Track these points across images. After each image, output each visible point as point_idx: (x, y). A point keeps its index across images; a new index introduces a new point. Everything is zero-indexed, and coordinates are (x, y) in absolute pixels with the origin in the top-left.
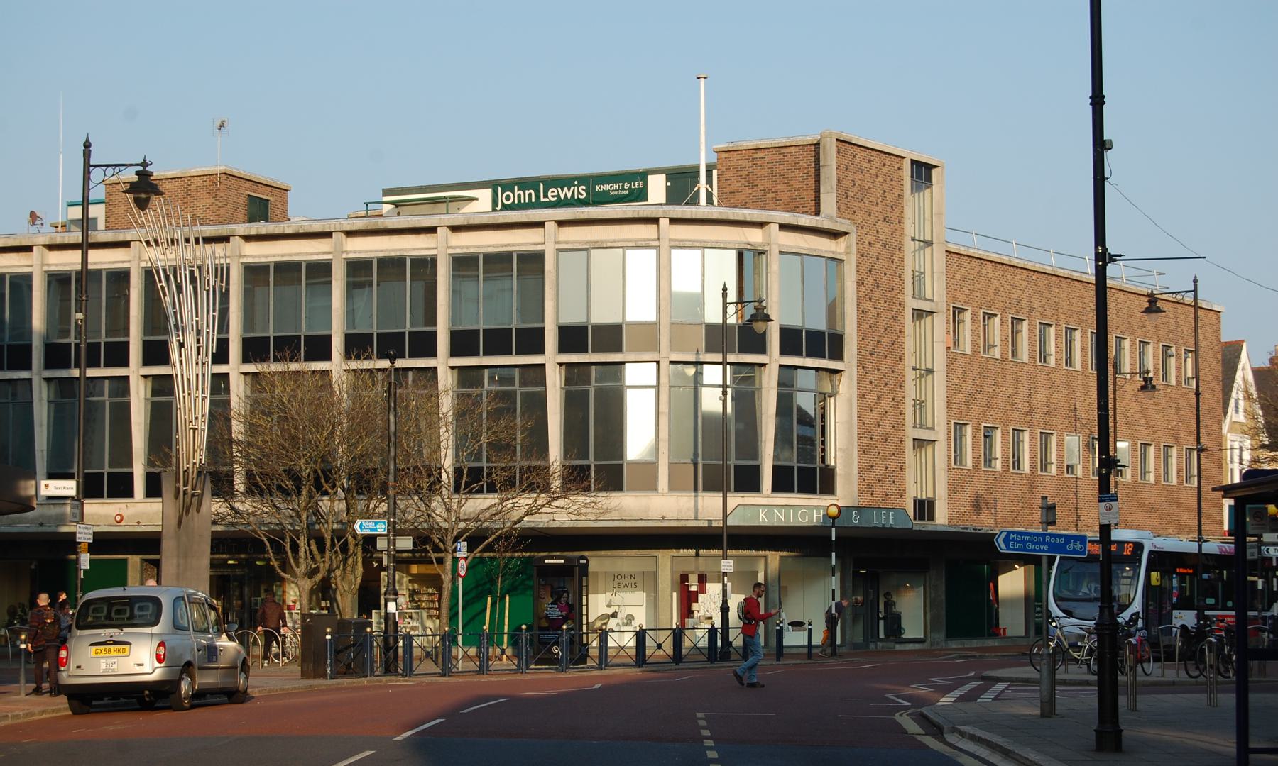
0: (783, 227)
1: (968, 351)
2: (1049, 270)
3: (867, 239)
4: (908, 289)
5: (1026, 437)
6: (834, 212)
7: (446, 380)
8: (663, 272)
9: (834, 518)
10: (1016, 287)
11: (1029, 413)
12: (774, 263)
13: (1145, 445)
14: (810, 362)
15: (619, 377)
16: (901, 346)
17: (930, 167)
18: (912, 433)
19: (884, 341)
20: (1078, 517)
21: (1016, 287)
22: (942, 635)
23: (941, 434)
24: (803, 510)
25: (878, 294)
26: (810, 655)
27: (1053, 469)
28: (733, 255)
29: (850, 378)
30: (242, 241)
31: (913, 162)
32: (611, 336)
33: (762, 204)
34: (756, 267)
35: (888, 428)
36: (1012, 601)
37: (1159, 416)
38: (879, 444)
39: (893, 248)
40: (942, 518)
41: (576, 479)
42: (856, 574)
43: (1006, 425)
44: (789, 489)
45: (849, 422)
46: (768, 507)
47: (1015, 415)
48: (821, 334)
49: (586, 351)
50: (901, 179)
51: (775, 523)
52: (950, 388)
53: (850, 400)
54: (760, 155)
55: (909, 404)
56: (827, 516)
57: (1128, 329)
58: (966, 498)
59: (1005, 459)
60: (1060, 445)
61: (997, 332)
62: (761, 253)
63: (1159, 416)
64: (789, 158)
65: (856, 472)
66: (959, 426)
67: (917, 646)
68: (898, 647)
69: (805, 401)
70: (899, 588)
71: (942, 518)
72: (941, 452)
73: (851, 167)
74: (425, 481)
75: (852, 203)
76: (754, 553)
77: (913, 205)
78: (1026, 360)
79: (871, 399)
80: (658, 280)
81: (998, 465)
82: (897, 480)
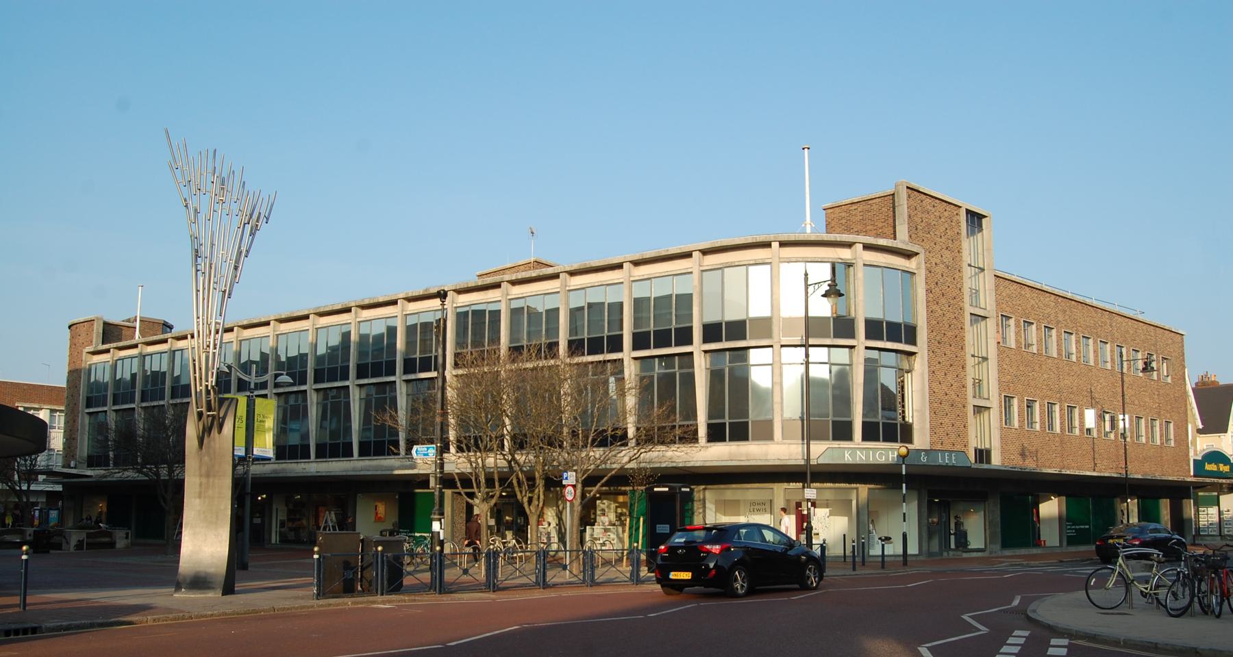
0: (867, 247)
1: (1013, 346)
2: (1069, 295)
3: (934, 261)
4: (967, 299)
5: (1057, 408)
6: (907, 238)
7: (631, 371)
9: (904, 457)
10: (1047, 306)
11: (1059, 392)
12: (860, 273)
14: (889, 345)
15: (745, 359)
16: (963, 339)
18: (972, 402)
21: (1047, 306)
22: (998, 546)
23: (994, 402)
24: (884, 453)
25: (943, 300)
26: (905, 563)
27: (1077, 432)
28: (828, 267)
29: (922, 358)
30: (509, 286)
31: (968, 211)
32: (737, 329)
33: (848, 230)
34: (847, 276)
35: (954, 397)
36: (1050, 520)
37: (1147, 399)
38: (946, 407)
39: (954, 269)
40: (996, 461)
41: (716, 434)
42: (931, 504)
43: (1042, 399)
44: (875, 438)
45: (923, 390)
46: (859, 451)
49: (721, 340)
50: (958, 222)
51: (858, 461)
52: (1001, 371)
53: (922, 374)
54: (854, 207)
55: (969, 383)
56: (899, 456)
57: (1125, 341)
58: (1014, 448)
59: (1042, 423)
60: (1082, 415)
61: (1034, 335)
62: (849, 265)
63: (1147, 399)
64: (875, 207)
65: (928, 426)
66: (1008, 399)
67: (980, 554)
68: (965, 555)
69: (887, 378)
70: (966, 512)
71: (996, 461)
72: (995, 416)
74: (622, 439)
75: (920, 234)
76: (847, 485)
77: (967, 245)
78: (1055, 355)
79: (940, 375)
80: (779, 291)
81: (1038, 427)
82: (962, 434)
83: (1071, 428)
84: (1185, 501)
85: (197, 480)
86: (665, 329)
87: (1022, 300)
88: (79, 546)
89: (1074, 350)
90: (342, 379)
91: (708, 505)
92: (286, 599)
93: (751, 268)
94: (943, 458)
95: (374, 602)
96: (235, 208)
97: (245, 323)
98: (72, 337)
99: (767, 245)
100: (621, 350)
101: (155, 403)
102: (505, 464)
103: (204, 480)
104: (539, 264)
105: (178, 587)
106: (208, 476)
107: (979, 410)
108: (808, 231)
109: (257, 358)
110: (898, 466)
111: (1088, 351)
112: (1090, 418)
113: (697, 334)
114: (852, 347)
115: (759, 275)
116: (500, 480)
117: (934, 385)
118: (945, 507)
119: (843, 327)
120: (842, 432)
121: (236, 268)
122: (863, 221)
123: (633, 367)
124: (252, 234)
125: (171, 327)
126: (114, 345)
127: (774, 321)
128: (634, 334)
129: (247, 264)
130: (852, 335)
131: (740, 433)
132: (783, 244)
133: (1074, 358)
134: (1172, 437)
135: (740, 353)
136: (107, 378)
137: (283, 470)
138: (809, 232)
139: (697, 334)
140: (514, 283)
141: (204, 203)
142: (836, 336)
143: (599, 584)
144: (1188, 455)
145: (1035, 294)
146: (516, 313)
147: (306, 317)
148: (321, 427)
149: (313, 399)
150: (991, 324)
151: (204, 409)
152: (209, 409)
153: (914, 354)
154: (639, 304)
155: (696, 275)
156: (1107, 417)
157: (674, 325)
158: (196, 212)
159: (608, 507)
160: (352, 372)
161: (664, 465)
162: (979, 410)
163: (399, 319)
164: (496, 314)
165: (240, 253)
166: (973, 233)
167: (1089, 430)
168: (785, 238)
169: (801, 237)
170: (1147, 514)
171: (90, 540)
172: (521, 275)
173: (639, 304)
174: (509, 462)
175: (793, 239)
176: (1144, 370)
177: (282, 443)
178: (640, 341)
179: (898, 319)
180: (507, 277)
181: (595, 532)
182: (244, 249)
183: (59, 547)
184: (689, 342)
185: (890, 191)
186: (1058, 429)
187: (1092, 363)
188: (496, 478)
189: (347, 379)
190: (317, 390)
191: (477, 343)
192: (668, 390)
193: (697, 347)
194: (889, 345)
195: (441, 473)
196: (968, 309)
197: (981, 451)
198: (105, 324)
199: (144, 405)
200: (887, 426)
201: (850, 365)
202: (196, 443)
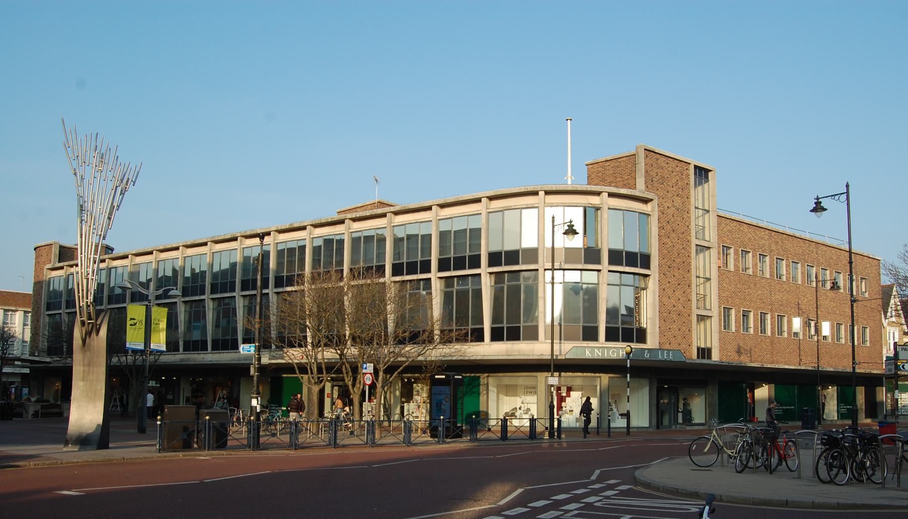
0: (611, 195)
3: (666, 205)
5: (769, 317)
7: (437, 287)
8: (541, 220)
12: (605, 214)
13: (839, 325)
14: (627, 269)
16: (689, 264)
17: (707, 171)
19: (678, 261)
20: (801, 360)
24: (617, 350)
25: (673, 235)
26: (628, 433)
27: (785, 335)
28: (581, 210)
29: (654, 279)
30: (351, 222)
31: (696, 167)
32: (513, 257)
34: (596, 217)
35: (681, 308)
38: (675, 317)
39: (683, 212)
40: (716, 357)
43: (756, 309)
46: (603, 349)
47: (762, 305)
48: (635, 254)
50: (688, 175)
51: (596, 357)
52: (721, 288)
53: (654, 291)
57: (829, 265)
60: (790, 323)
61: (751, 261)
62: (598, 209)
64: (623, 164)
66: (727, 310)
67: (701, 427)
68: (688, 428)
70: (692, 396)
71: (716, 357)
72: (715, 324)
73: (655, 165)
75: (656, 185)
78: (768, 276)
79: (669, 292)
80: (537, 227)
81: (752, 331)
82: (687, 336)
83: (781, 332)
84: (878, 388)
85: (82, 368)
86: (461, 255)
87: (738, 234)
88: (36, 415)
89: (785, 272)
90: (253, 289)
91: (490, 388)
92: (145, 452)
93: (523, 211)
94: (663, 355)
95: (200, 455)
96: (110, 175)
97: (161, 248)
98: (37, 257)
99: (536, 193)
100: (429, 271)
101: (197, 298)
102: (338, 357)
103: (86, 368)
104: (382, 204)
105: (66, 443)
106: (89, 365)
107: (702, 318)
108: (569, 183)
109: (169, 273)
110: (625, 360)
111: (796, 274)
112: (797, 323)
113: (484, 260)
114: (599, 271)
115: (530, 218)
116: (327, 368)
117: (664, 299)
118: (674, 391)
119: (591, 255)
120: (590, 334)
121: (109, 218)
122: (610, 175)
123: (438, 285)
124: (122, 193)
125: (112, 250)
126: (67, 263)
127: (540, 252)
128: (393, 265)
129: (117, 215)
130: (598, 262)
131: (514, 335)
132: (547, 193)
133: (784, 278)
134: (868, 339)
135: (515, 274)
136: (62, 288)
137: (188, 359)
138: (569, 184)
139: (484, 260)
140: (354, 220)
141: (89, 172)
142: (586, 262)
143: (415, 444)
144: (881, 353)
145: (752, 229)
146: (355, 241)
147: (205, 244)
148: (217, 326)
149: (210, 306)
150: (714, 252)
151: (85, 319)
152: (90, 318)
153: (647, 276)
154: (444, 235)
155: (484, 216)
156: (813, 324)
157: (468, 253)
158: (82, 179)
159: (422, 389)
160: (238, 286)
161: (454, 358)
162: (702, 318)
163: (272, 246)
164: (341, 242)
165: (112, 207)
166: (700, 184)
167: (796, 334)
168: (548, 188)
169: (561, 188)
170: (845, 399)
171: (44, 411)
172: (359, 214)
173: (444, 235)
174: (340, 355)
175: (554, 189)
176: (832, 288)
177: (187, 339)
178: (444, 265)
179: (635, 249)
180: (349, 216)
181: (410, 407)
182: (115, 204)
183: (20, 415)
184: (478, 266)
185: (633, 152)
186: (769, 332)
187: (800, 282)
188: (324, 367)
189: (234, 291)
190: (213, 299)
191: (329, 263)
192: (463, 305)
193: (484, 270)
194: (627, 269)
195: (259, 364)
196: (694, 241)
197: (703, 349)
198: (61, 247)
199: (69, 311)
200: (625, 328)
201: (598, 284)
202: (80, 342)
